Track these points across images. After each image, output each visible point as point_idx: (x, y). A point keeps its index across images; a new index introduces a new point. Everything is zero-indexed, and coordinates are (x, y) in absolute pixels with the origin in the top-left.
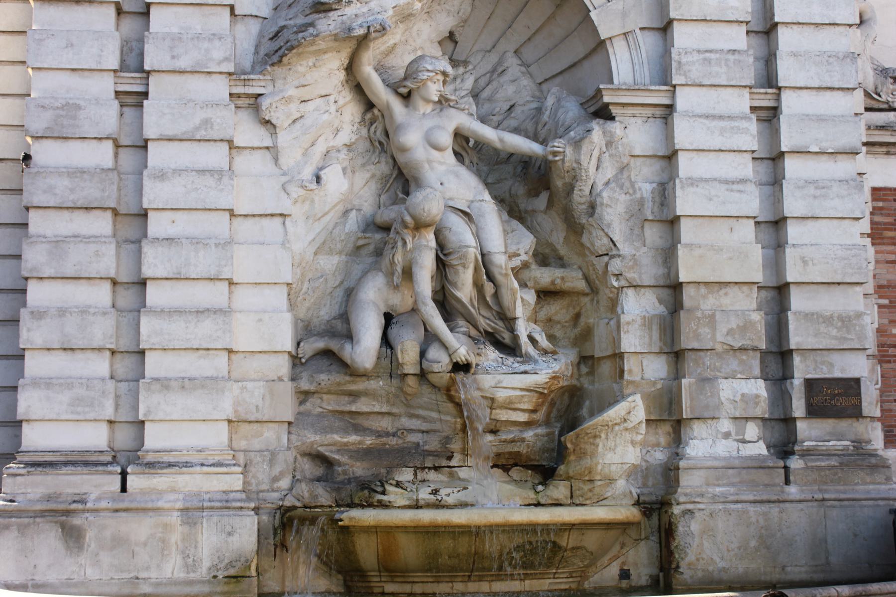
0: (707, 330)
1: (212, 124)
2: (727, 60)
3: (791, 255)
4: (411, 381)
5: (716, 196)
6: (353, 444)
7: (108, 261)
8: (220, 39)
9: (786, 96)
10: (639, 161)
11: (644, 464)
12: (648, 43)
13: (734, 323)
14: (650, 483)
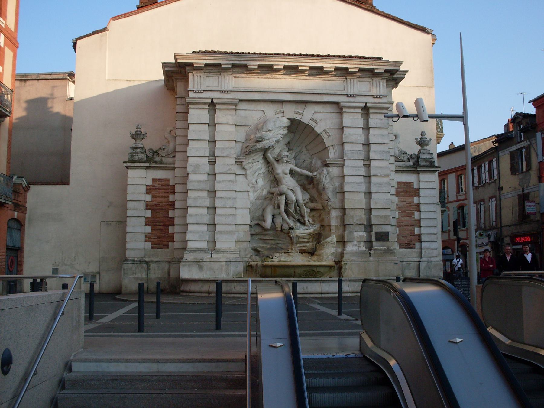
3: (372, 201)
4: (279, 231)
7: (207, 203)
9: (372, 162)
12: (338, 148)
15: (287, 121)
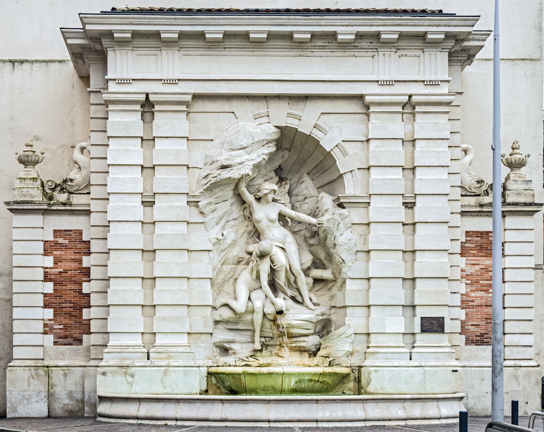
15: (276, 130)
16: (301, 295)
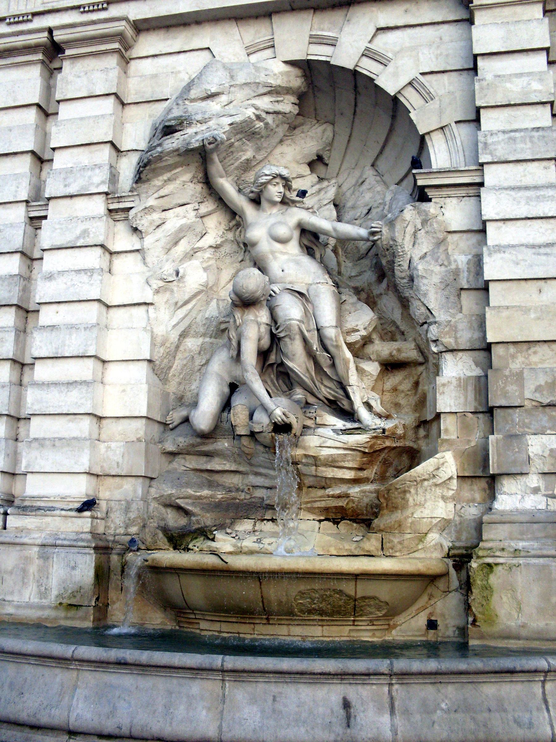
0: (515, 388)
1: (89, 233)
2: (531, 137)
5: (523, 260)
6: (206, 498)
8: (99, 168)
10: (456, 237)
11: (457, 518)
13: (542, 380)
14: (464, 537)
16: (348, 396)
